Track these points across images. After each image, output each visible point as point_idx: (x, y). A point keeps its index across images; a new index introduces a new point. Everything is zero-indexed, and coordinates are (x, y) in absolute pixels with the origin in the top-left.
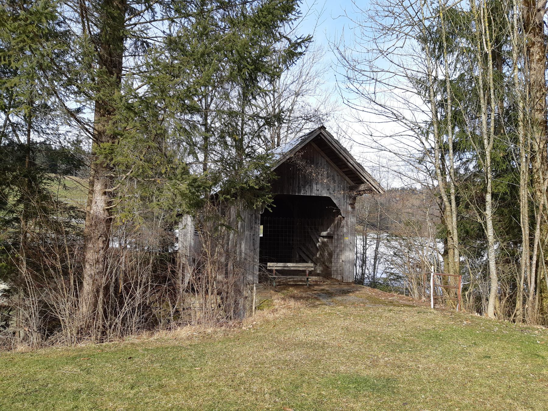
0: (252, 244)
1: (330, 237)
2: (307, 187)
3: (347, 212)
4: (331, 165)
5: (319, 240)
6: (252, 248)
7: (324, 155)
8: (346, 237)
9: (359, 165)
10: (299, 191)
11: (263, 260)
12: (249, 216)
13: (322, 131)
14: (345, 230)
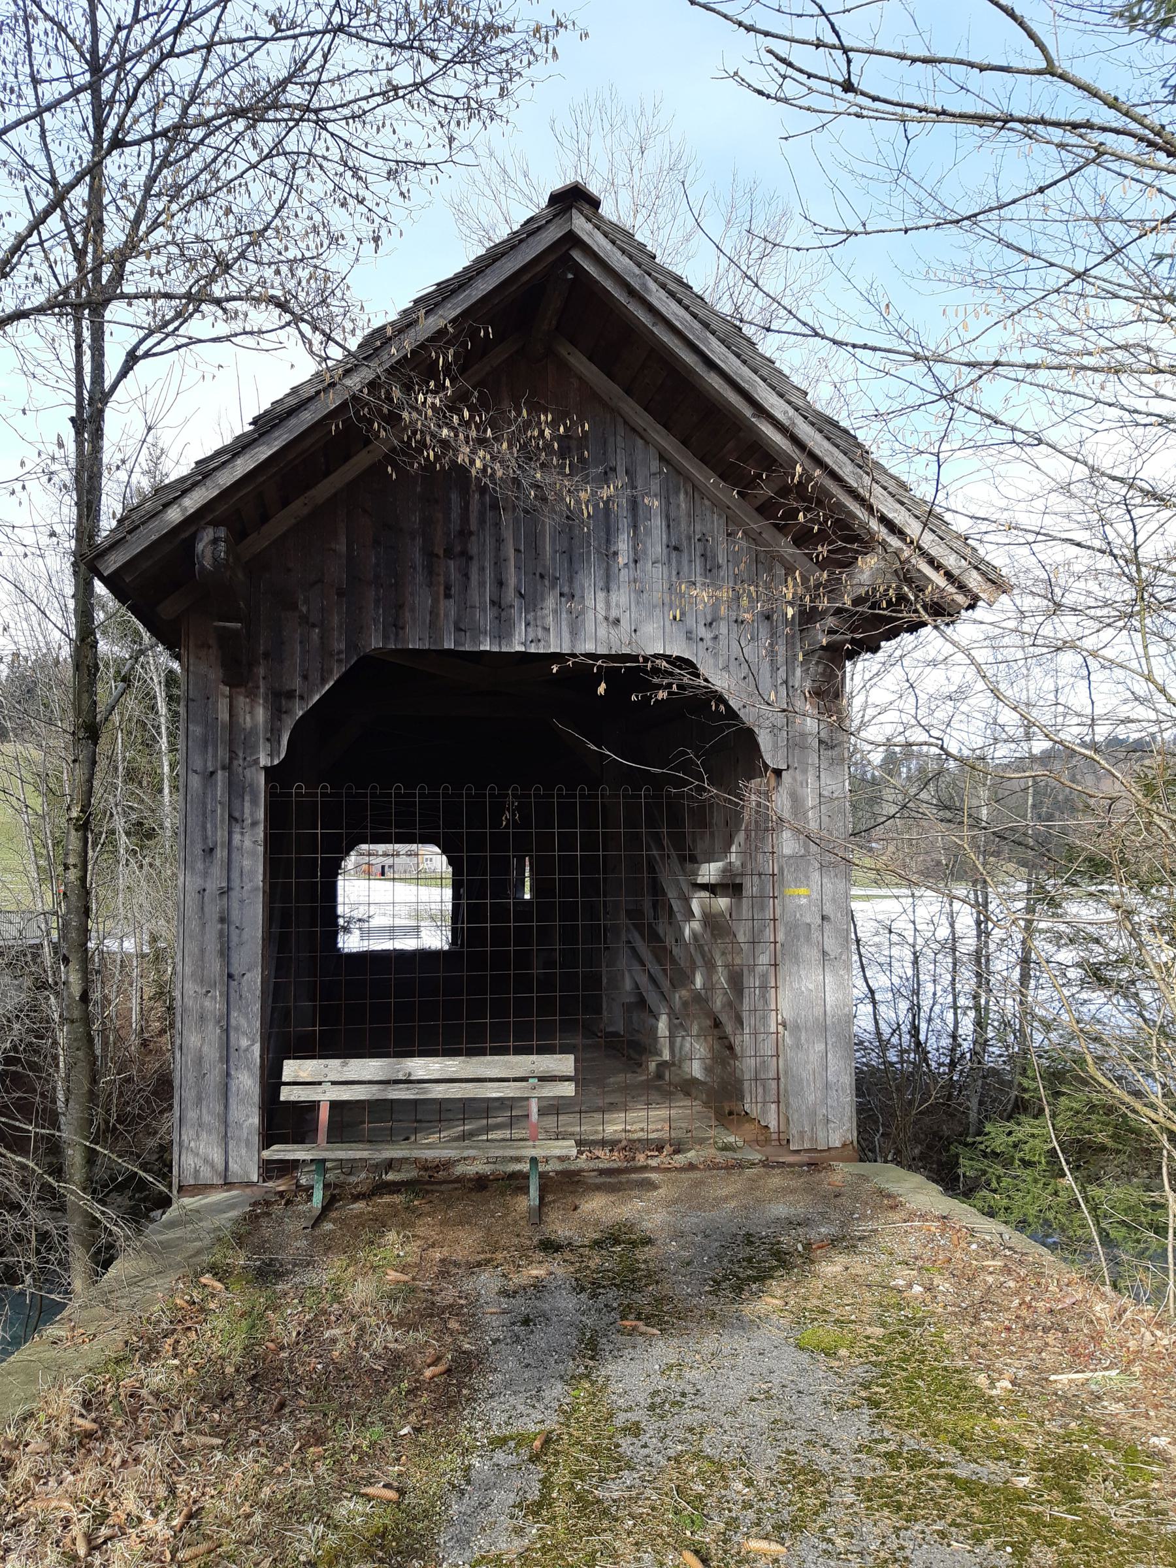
0: (212, 946)
1: (731, 886)
2: (550, 602)
3: (796, 744)
4: (688, 478)
5: (695, 906)
6: (215, 967)
7: (642, 419)
8: (798, 883)
9: (828, 426)
10: (503, 629)
11: (283, 1042)
12: (195, 781)
13: (580, 225)
14: (788, 844)
